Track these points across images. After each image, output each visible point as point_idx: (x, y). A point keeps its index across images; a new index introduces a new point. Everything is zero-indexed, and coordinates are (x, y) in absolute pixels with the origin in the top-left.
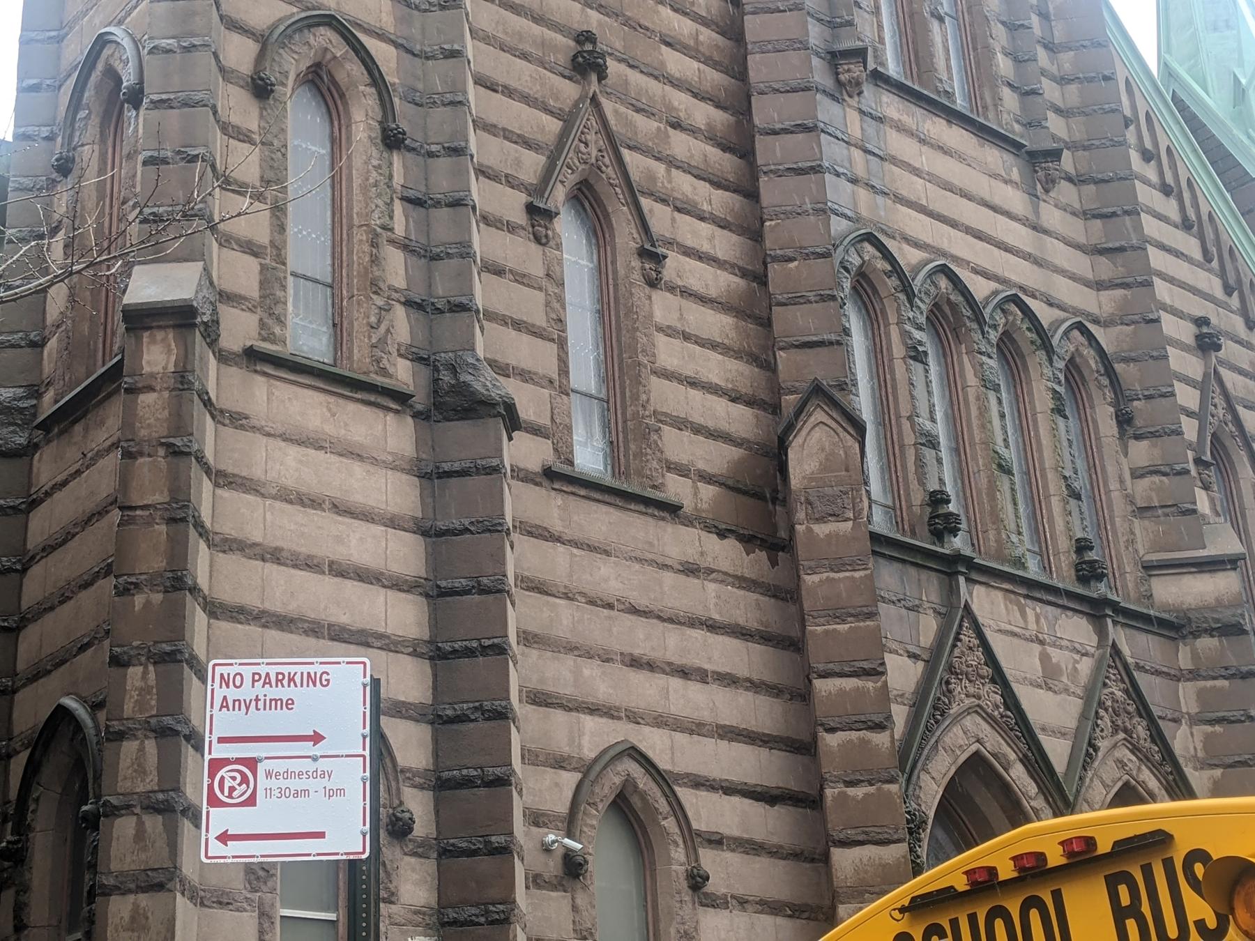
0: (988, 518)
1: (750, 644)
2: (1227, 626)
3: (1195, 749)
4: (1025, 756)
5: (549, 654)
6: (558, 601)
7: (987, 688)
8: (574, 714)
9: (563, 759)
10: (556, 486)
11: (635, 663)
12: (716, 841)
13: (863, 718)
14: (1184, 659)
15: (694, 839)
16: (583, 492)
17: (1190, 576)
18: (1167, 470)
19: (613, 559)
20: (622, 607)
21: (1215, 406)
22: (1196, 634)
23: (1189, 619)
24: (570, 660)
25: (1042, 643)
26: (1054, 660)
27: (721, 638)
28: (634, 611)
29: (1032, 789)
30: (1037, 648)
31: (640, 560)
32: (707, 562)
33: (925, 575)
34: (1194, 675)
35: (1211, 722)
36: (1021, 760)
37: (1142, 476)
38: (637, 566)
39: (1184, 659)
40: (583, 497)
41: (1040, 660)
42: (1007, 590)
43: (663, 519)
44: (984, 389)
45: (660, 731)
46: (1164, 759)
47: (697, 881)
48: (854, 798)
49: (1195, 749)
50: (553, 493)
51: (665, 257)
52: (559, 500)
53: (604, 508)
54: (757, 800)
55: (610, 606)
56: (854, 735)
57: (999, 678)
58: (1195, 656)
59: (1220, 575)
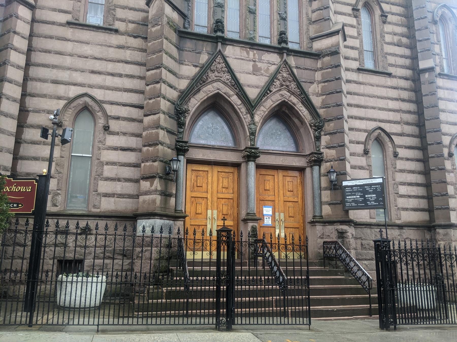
1: (141, 67)
2: (333, 52)
4: (237, 93)
5: (61, 70)
7: (225, 75)
8: (68, 86)
9: (61, 97)
10: (70, 26)
11: (93, 72)
12: (401, 147)
14: (319, 65)
15: (107, 117)
16: (81, 27)
18: (322, 8)
19: (90, 45)
20: (91, 58)
22: (324, 57)
23: (322, 53)
24: (68, 72)
25: (254, 61)
26: (259, 66)
28: (96, 58)
29: (239, 102)
30: (252, 63)
31: (101, 45)
32: (129, 45)
33: (205, 43)
34: (321, 69)
35: (324, 82)
36: (236, 95)
37: (315, 12)
38: (99, 47)
39: (319, 65)
41: (253, 66)
42: (241, 46)
45: (101, 90)
46: (302, 93)
47: (396, 155)
48: (150, 103)
49: (318, 91)
50: (70, 28)
51: (387, 16)
52: (71, 30)
53: (89, 32)
54: (409, 136)
55: (86, 57)
56: (152, 86)
57: (230, 71)
58: (323, 63)
59: (334, 37)
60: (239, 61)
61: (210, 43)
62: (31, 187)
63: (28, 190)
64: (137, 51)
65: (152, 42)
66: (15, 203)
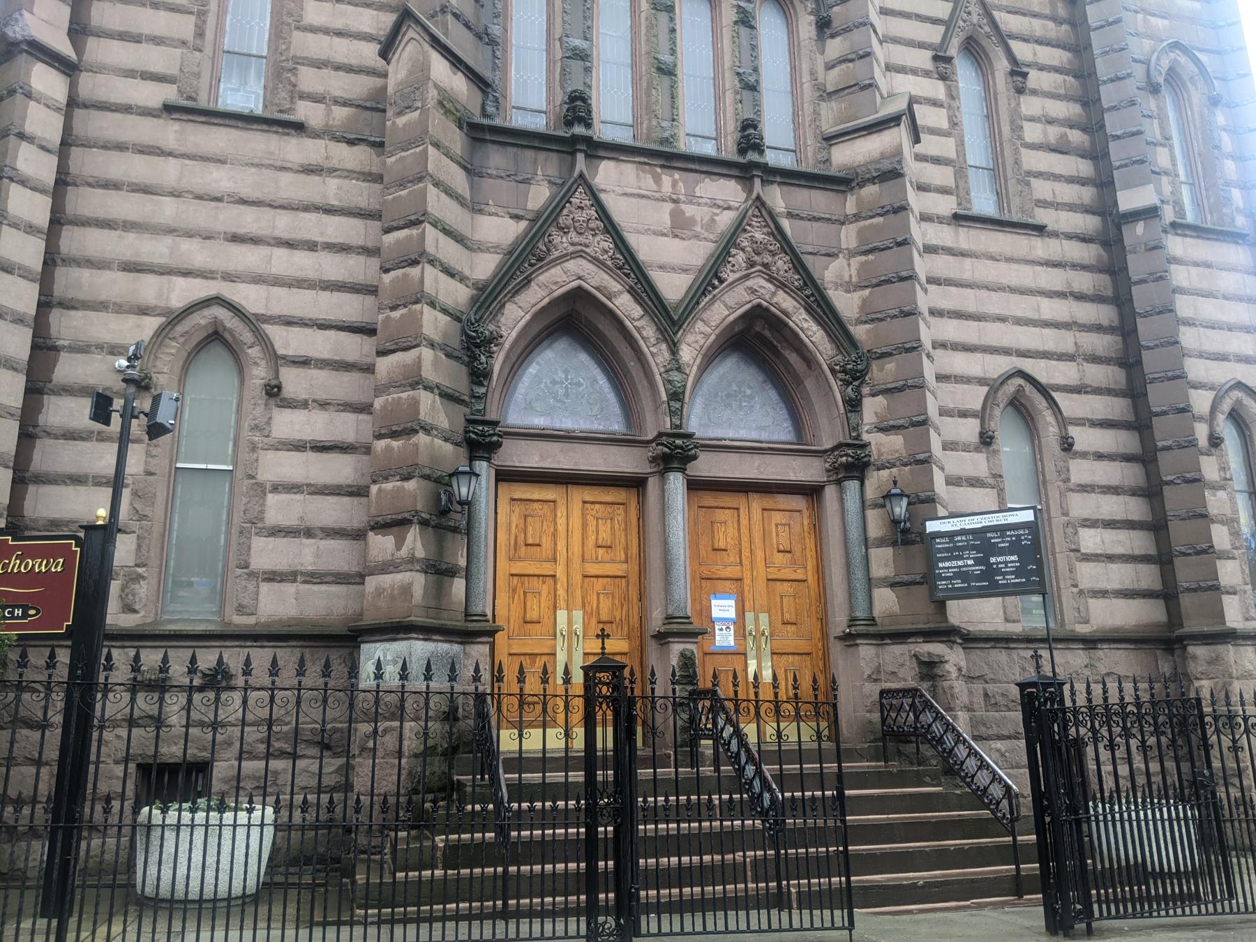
0: (644, 111)
1: (369, 221)
3: (851, 276)
4: (631, 287)
6: (163, 198)
7: (598, 238)
8: (166, 277)
9: (148, 308)
13: (406, 258)
14: (851, 205)
15: (276, 360)
16: (203, 119)
17: (862, 139)
18: (853, 56)
19: (228, 166)
20: (230, 200)
21: (969, 13)
22: (861, 185)
23: (857, 174)
24: (169, 240)
25: (675, 201)
26: (687, 214)
27: (337, 218)
28: (243, 202)
29: (637, 311)
32: (334, 163)
34: (857, 217)
35: (866, 253)
36: (629, 292)
37: (833, 66)
38: (253, 170)
40: (202, 122)
43: (288, 134)
44: (654, 11)
45: (258, 287)
46: (805, 284)
49: (851, 276)
50: (171, 122)
52: (176, 126)
56: (400, 272)
57: (611, 229)
58: (860, 202)
59: (886, 132)
62: (61, 560)
63: (56, 567)
64: (358, 179)
65: (398, 156)
66: (18, 607)
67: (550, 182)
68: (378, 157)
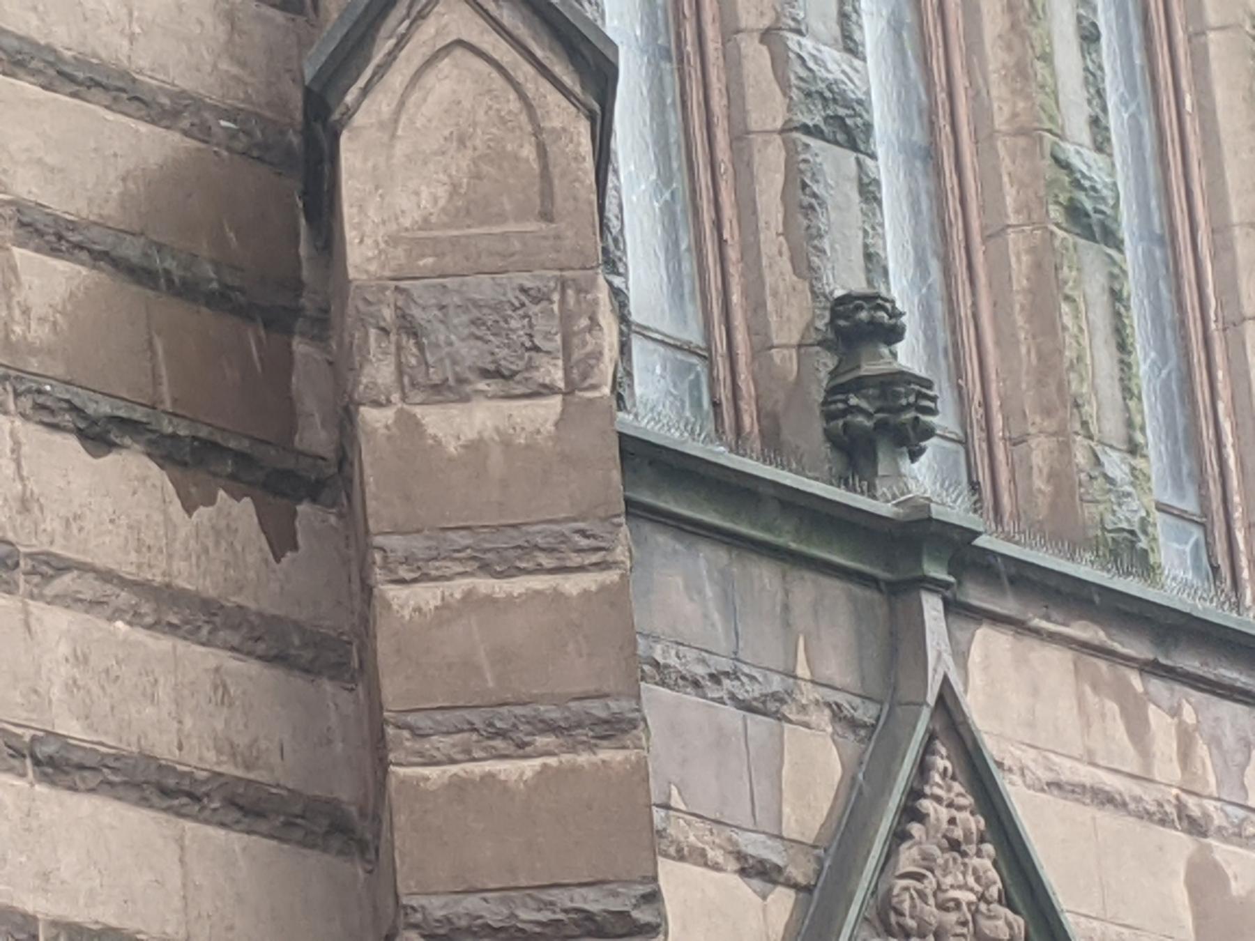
1: (189, 825)
25: (1196, 827)
26: (1236, 888)
30: (1180, 843)
60: (1087, 813)
61: (835, 588)
64: (135, 619)
65: (459, 587)
67: (837, 713)
68: (189, 509)
